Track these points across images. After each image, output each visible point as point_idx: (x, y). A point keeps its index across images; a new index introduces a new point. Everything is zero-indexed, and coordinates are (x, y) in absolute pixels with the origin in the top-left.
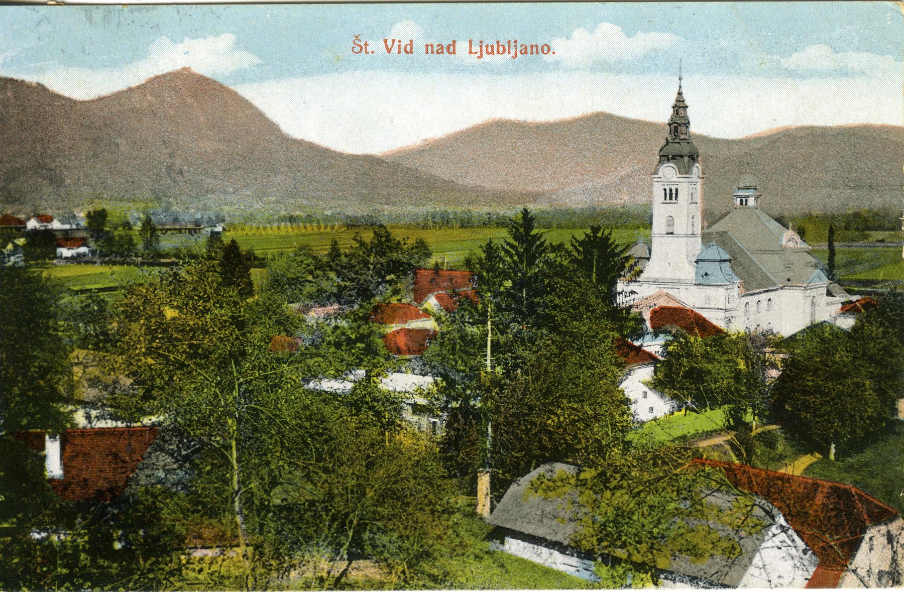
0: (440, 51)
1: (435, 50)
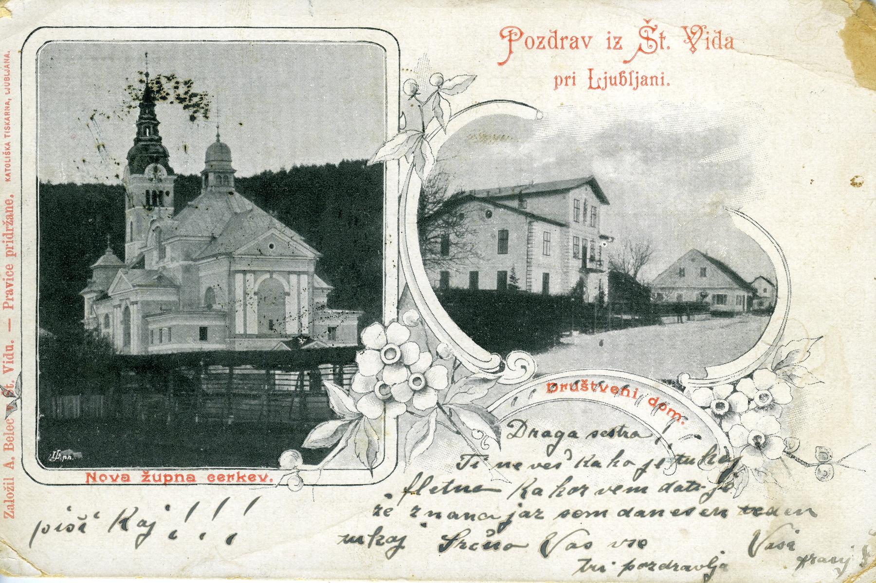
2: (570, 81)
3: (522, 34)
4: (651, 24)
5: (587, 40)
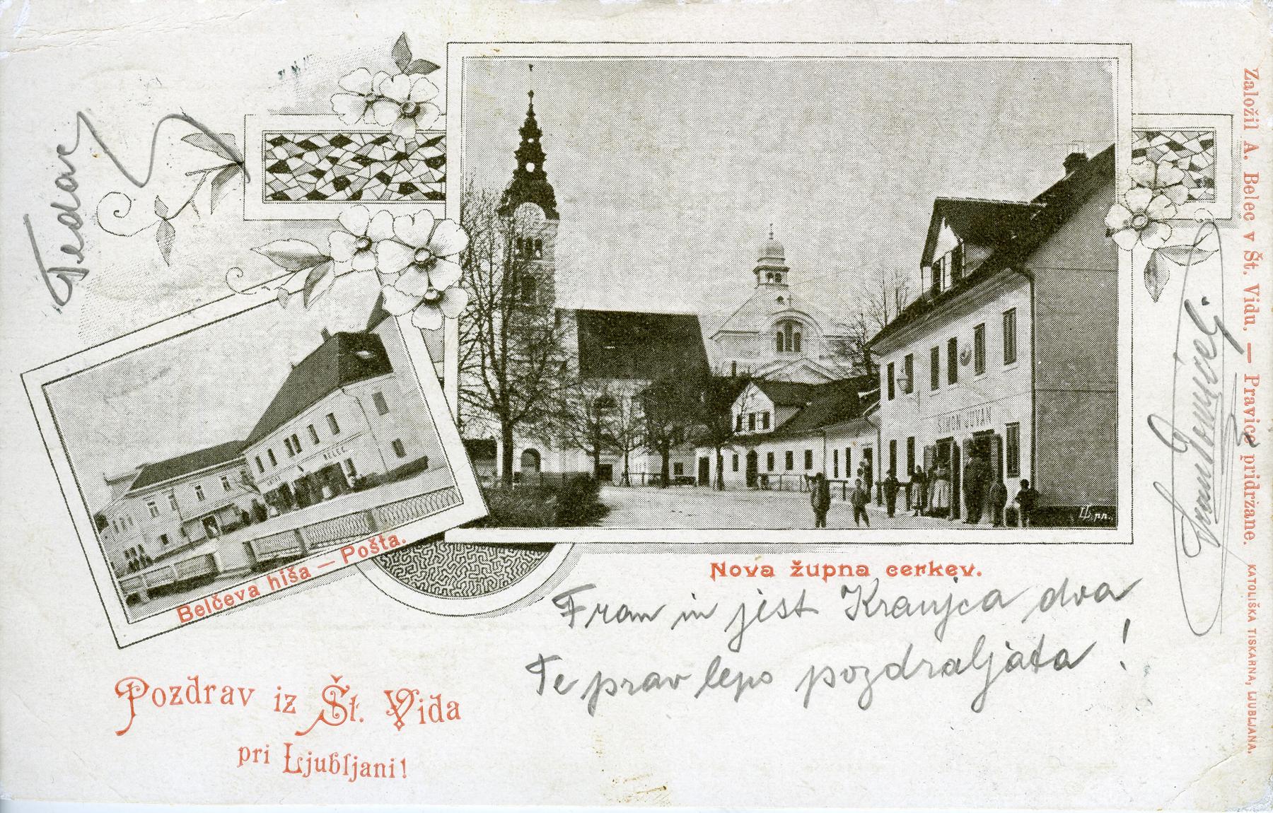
2: (261, 757)
3: (146, 687)
4: (341, 683)
5: (246, 693)
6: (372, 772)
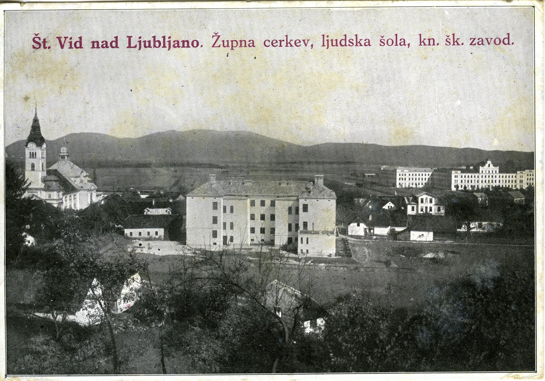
0: (105, 45)
1: (100, 46)
5: (306, 42)
6: (181, 44)
